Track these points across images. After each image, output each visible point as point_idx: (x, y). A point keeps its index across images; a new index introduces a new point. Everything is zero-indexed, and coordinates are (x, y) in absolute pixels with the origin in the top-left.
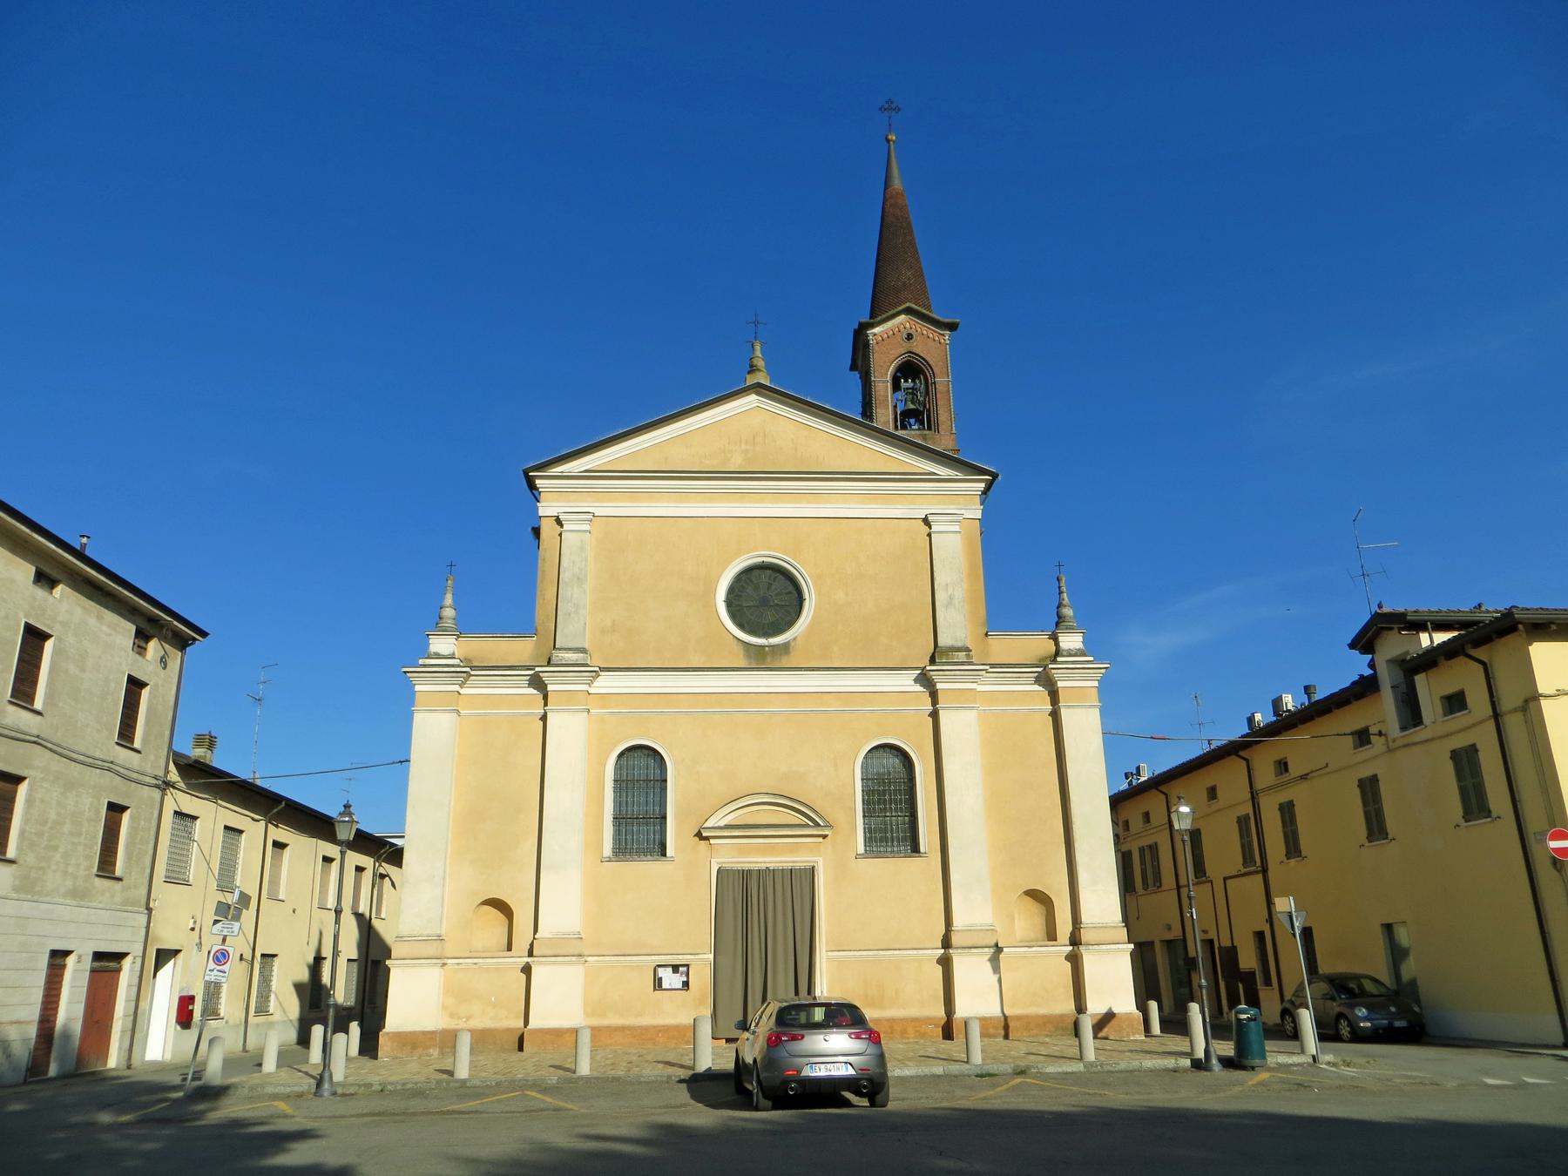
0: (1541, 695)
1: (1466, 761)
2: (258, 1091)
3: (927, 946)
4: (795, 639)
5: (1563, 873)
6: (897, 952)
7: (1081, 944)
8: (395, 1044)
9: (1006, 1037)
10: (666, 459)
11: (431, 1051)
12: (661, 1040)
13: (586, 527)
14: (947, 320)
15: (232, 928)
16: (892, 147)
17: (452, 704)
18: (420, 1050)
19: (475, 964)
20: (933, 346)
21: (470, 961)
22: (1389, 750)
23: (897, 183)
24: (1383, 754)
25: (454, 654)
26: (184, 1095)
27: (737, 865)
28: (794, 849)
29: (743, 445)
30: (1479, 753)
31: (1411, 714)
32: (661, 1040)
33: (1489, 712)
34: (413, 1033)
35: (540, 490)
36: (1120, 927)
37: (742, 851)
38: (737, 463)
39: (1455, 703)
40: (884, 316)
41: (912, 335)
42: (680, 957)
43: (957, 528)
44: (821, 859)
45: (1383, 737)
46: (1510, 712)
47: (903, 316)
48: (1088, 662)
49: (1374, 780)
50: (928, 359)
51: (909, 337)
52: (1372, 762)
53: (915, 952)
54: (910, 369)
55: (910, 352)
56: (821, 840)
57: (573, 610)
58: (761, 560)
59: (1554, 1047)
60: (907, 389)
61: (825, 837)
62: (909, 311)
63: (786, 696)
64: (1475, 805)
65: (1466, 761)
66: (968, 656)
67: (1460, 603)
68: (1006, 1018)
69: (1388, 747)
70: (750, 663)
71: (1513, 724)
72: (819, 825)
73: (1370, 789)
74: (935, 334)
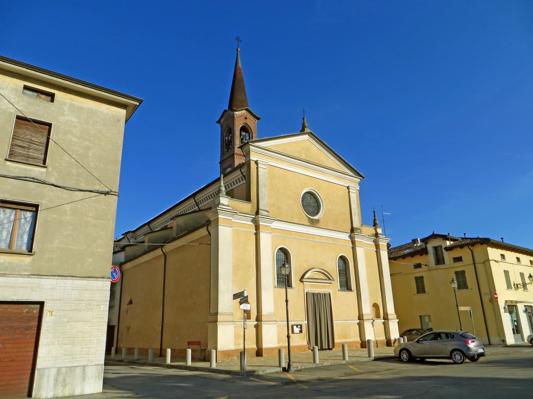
0: (490, 260)
1: (461, 276)
2: (265, 372)
3: (339, 320)
4: (320, 218)
5: (493, 303)
6: (349, 321)
7: (262, 321)
8: (222, 355)
9: (377, 347)
10: (285, 149)
11: (234, 357)
12: (296, 351)
13: (265, 167)
14: (258, 116)
15: (247, 307)
16: (239, 53)
17: (230, 224)
18: (231, 357)
19: (240, 324)
20: (252, 123)
21: (239, 323)
22: (430, 270)
23: (240, 65)
24: (427, 271)
25: (228, 205)
26: (250, 378)
27: (311, 291)
28: (324, 287)
29: (305, 151)
30: (466, 273)
31: (439, 260)
32: (296, 351)
33: (473, 263)
34: (228, 351)
35: (250, 150)
36: (394, 314)
37: (312, 287)
38: (303, 157)
39: (458, 259)
40: (241, 109)
41: (247, 118)
42: (299, 322)
43: (355, 192)
44: (331, 291)
45: (427, 266)
46: (479, 263)
47: (244, 111)
48: (384, 237)
49: (422, 278)
50: (251, 127)
51: (246, 118)
52: (419, 273)
53: (353, 321)
54: (244, 129)
55: (246, 123)
56: (330, 284)
57: (264, 196)
58: (310, 190)
59: (487, 345)
60: (243, 135)
61: (331, 283)
62: (247, 110)
63: (319, 237)
64: (463, 285)
65: (461, 276)
66: (360, 231)
67: (458, 235)
68: (377, 341)
69: (429, 269)
70: (310, 224)
71: (480, 267)
72: (331, 280)
73: (419, 280)
74: (253, 120)
